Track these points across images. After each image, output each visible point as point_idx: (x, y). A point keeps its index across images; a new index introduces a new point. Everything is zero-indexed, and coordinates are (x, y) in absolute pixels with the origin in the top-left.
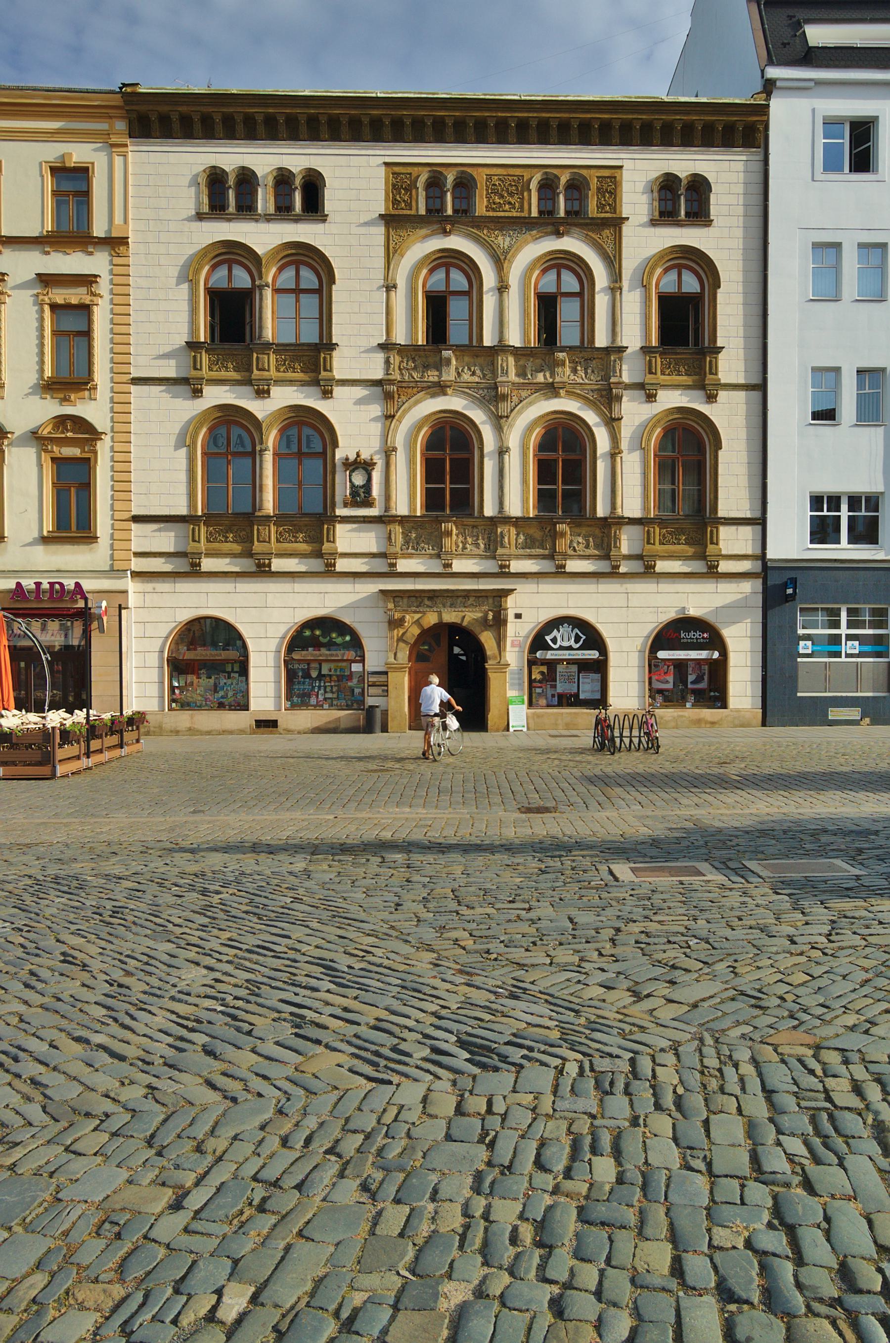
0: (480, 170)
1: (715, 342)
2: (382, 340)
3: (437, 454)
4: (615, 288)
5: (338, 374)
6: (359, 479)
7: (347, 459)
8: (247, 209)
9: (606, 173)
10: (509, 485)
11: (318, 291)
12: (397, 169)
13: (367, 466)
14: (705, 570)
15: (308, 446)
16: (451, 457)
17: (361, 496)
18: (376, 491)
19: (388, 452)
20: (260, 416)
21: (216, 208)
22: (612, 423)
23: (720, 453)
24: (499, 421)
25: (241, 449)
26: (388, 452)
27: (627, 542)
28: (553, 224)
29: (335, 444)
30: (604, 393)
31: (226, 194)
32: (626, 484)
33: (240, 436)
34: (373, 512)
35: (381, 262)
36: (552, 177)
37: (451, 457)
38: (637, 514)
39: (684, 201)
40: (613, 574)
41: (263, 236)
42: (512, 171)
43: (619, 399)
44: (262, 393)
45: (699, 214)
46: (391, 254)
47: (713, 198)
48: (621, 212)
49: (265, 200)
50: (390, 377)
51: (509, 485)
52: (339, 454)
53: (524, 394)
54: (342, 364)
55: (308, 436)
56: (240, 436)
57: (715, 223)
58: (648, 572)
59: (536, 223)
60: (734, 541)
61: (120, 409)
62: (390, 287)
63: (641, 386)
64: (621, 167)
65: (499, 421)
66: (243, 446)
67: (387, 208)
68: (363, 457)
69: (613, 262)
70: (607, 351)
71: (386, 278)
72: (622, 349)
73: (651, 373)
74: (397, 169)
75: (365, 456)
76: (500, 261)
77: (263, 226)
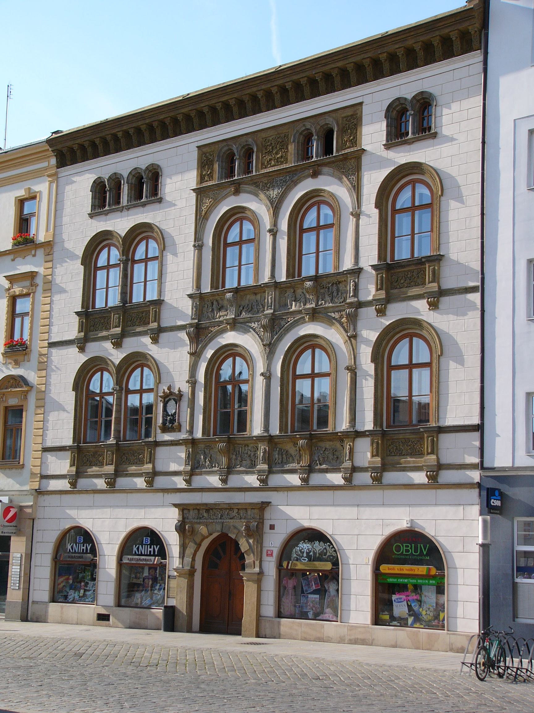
6: (171, 410)
9: (349, 112)
15: (146, 385)
19: (193, 382)
31: (105, 196)
34: (183, 435)
39: (413, 119)
41: (121, 224)
60: (459, 450)
61: (43, 366)
62: (199, 247)
64: (361, 104)
67: (197, 184)
74: (204, 150)
76: (275, 208)
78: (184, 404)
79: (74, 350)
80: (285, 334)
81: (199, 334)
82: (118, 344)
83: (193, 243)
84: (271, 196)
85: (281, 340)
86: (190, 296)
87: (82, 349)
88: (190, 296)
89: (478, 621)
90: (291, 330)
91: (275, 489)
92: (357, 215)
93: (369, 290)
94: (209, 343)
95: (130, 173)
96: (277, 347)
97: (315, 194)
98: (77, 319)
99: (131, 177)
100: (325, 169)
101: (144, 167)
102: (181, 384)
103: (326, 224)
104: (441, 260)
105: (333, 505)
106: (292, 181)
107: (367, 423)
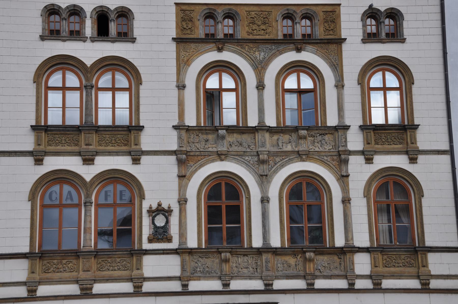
0: (242, 7)
1: (413, 121)
2: (176, 123)
3: (214, 203)
4: (340, 85)
5: (144, 147)
6: (160, 221)
7: (151, 208)
8: (76, 35)
9: (329, 9)
10: (266, 225)
11: (129, 89)
12: (184, 7)
13: (167, 213)
14: (419, 287)
15: (121, 199)
16: (224, 206)
17: (161, 234)
18: (174, 230)
19: (183, 202)
20: (88, 178)
21: (52, 34)
22: (343, 178)
23: (423, 200)
24: (264, 179)
25: (69, 202)
26: (183, 202)
27: (362, 264)
28: (293, 43)
29: (142, 197)
30: (335, 158)
32: (353, 220)
33: (69, 193)
34: (174, 245)
35: (174, 70)
36: (292, 12)
37: (224, 206)
38: (366, 244)
40: (351, 289)
42: (263, 8)
43: (346, 162)
44: (88, 161)
45: (396, 36)
46: (182, 64)
47: (405, 24)
48: (340, 35)
49: (89, 28)
50: (182, 149)
51: (266, 225)
52: (146, 205)
53: (278, 159)
54: (147, 142)
55: (121, 192)
56: (69, 193)
57: (407, 41)
58: (377, 288)
59: (282, 43)
62: (181, 87)
63: (362, 153)
65: (264, 179)
66: (72, 199)
67: (177, 34)
68: (163, 206)
69: (337, 67)
70: (336, 128)
71: (178, 81)
72: (347, 128)
73: (369, 144)
74: (184, 7)
75: (165, 206)
76: (260, 68)
77: (89, 44)
78: (174, 220)
79: (30, 160)
80: (280, 169)
81: (185, 160)
82: (88, 161)
83: (175, 83)
84: (258, 58)
85: (277, 173)
86: (175, 127)
87: (39, 161)
88: (175, 127)
89: (50, 105)
90: (286, 166)
91: (283, 292)
92: (340, 85)
93: (355, 141)
94: (199, 169)
95: (95, 9)
96: (273, 178)
97: (241, 77)
98: (175, 133)
99: (95, 13)
100: (309, 47)
101: (112, 8)
102: (170, 200)
103: (38, 125)
104: (417, 128)
105: (240, 235)
106: (278, 51)
107: (362, 238)
